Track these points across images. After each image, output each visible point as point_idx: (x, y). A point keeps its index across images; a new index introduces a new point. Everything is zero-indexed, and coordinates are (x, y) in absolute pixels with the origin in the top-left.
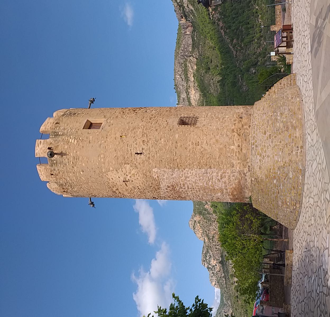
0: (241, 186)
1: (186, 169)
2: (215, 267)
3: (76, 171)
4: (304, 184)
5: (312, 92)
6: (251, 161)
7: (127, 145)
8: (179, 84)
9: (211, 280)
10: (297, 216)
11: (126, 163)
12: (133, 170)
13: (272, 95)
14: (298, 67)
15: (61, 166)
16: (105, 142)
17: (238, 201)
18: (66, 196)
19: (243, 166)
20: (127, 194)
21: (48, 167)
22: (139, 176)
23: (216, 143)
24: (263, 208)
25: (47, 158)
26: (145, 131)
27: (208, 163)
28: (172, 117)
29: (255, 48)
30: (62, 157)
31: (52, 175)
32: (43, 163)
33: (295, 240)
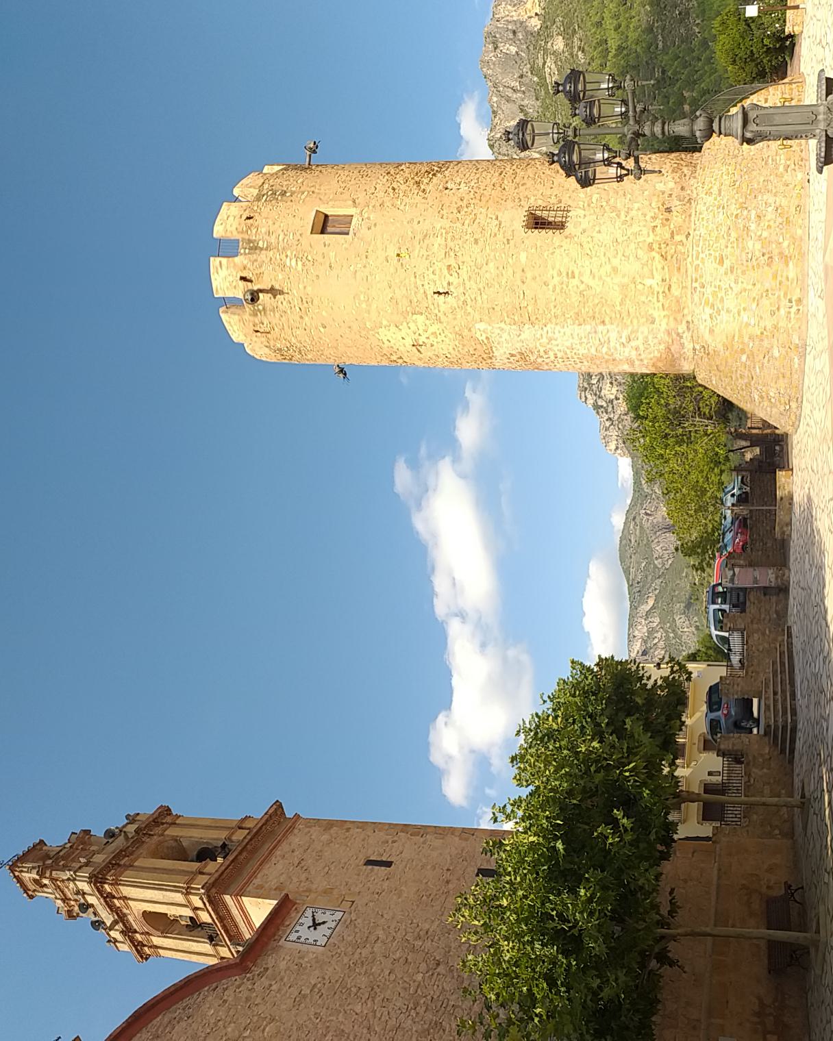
0: (673, 356)
2: (615, 402)
9: (604, 438)
16: (365, 267)
26: (451, 244)
28: (510, 204)
30: (275, 298)
31: (257, 331)
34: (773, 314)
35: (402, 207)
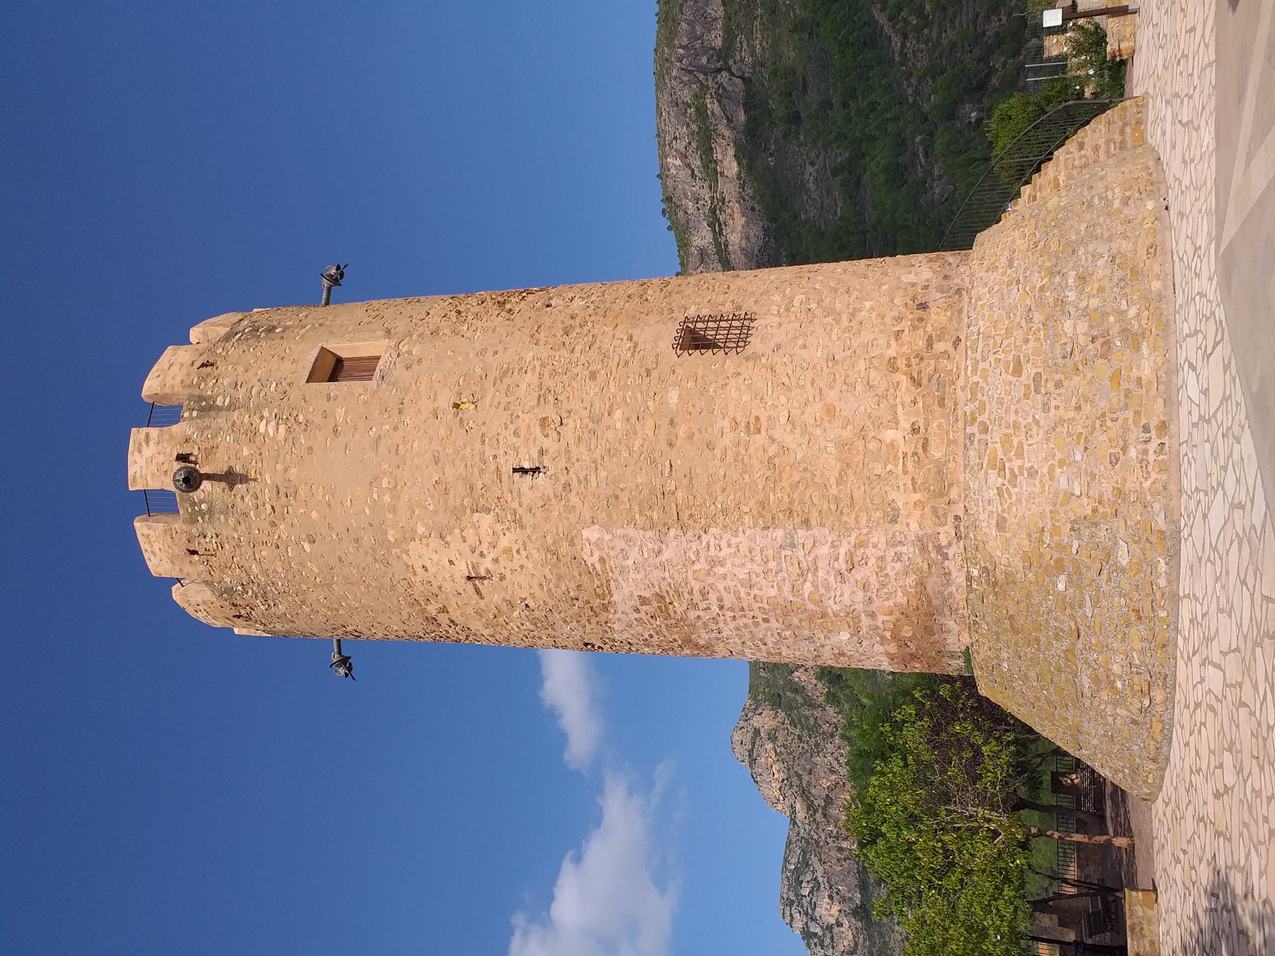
0: (930, 602)
1: (711, 529)
2: (836, 930)
3: (284, 537)
4: (1175, 598)
5: (1209, 166)
6: (963, 495)
7: (479, 440)
8: (679, 192)
10: (1159, 740)
11: (480, 506)
12: (507, 533)
13: (1046, 195)
14: (1156, 66)
15: (227, 520)
16: (396, 428)
17: (918, 667)
18: (245, 632)
19: (934, 518)
20: (480, 628)
21: (177, 526)
22: (527, 557)
23: (826, 419)
24: (1021, 701)
25: (173, 494)
26: (550, 383)
27: (799, 504)
28: (653, 318)
29: (978, 16)
31: (194, 552)
32: (160, 512)
33: (1163, 846)
34: (1114, 460)
35: (469, 334)
